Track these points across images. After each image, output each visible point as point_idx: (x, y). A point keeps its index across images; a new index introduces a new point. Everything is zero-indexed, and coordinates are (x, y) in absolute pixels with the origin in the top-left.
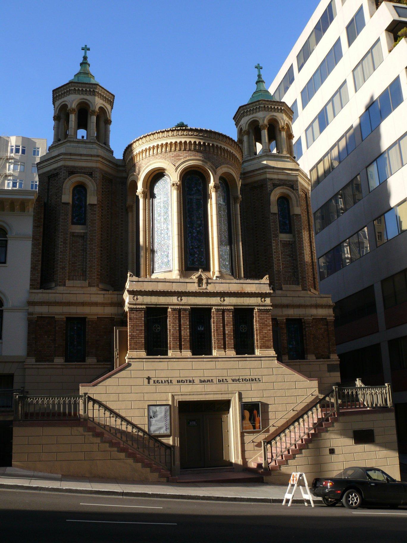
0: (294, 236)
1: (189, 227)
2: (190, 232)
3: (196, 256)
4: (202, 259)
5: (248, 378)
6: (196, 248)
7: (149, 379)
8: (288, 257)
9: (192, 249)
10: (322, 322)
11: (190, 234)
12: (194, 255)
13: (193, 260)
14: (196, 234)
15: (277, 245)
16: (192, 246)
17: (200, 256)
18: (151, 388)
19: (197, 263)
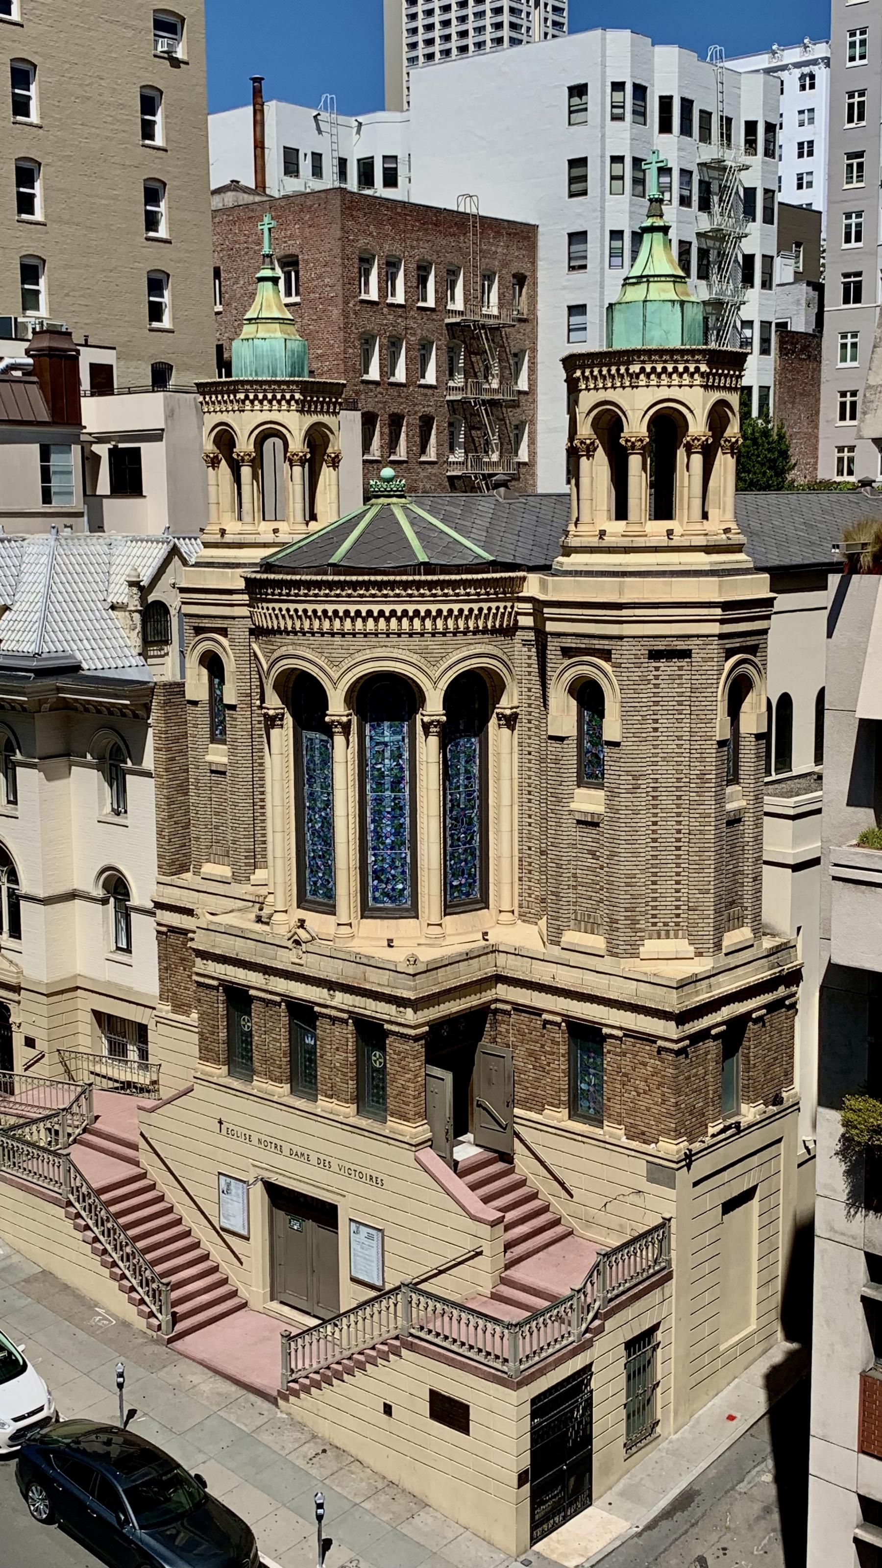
0: (612, 795)
1: (309, 808)
2: (310, 820)
3: (321, 875)
4: (329, 883)
5: (364, 1171)
6: (320, 857)
7: (221, 1122)
8: (590, 856)
9: (314, 858)
10: (648, 1048)
11: (310, 825)
12: (317, 872)
13: (315, 883)
14: (320, 825)
15: (559, 824)
16: (314, 851)
17: (326, 877)
18: (223, 1141)
19: (321, 892)
